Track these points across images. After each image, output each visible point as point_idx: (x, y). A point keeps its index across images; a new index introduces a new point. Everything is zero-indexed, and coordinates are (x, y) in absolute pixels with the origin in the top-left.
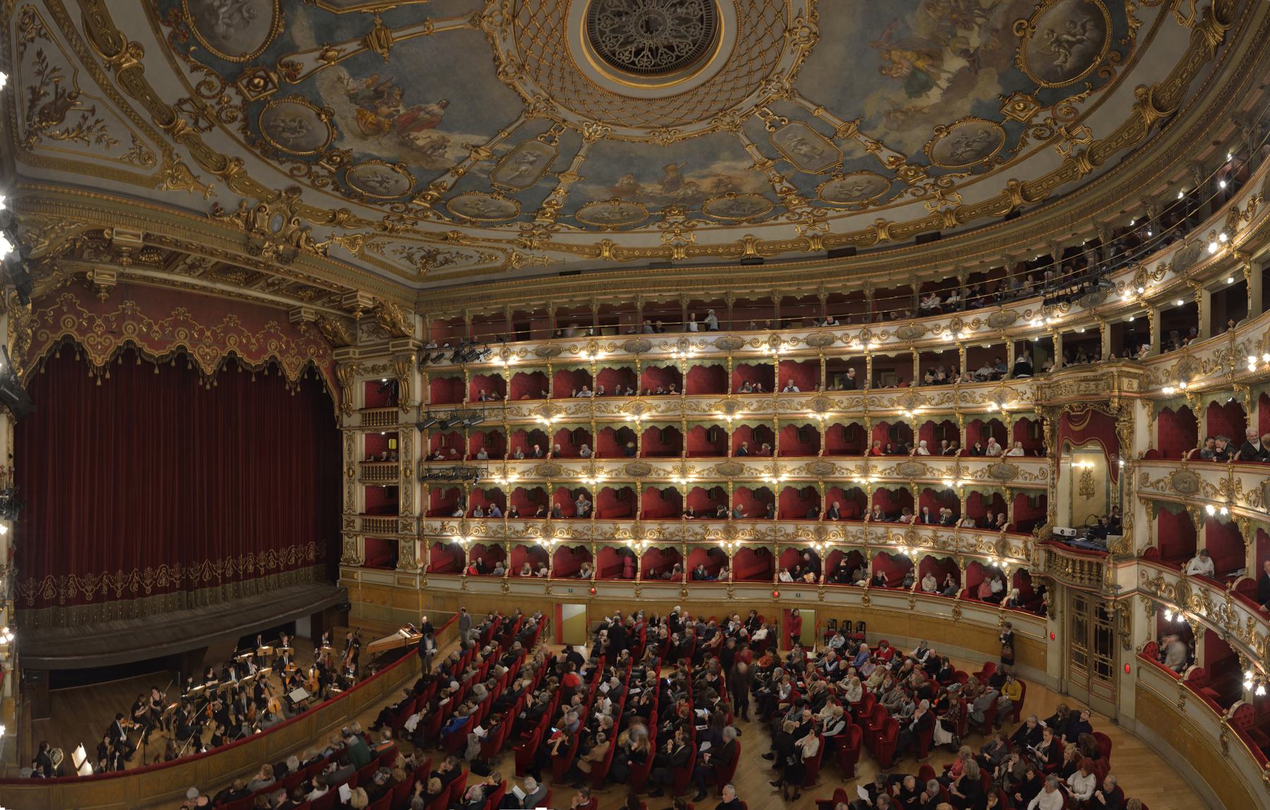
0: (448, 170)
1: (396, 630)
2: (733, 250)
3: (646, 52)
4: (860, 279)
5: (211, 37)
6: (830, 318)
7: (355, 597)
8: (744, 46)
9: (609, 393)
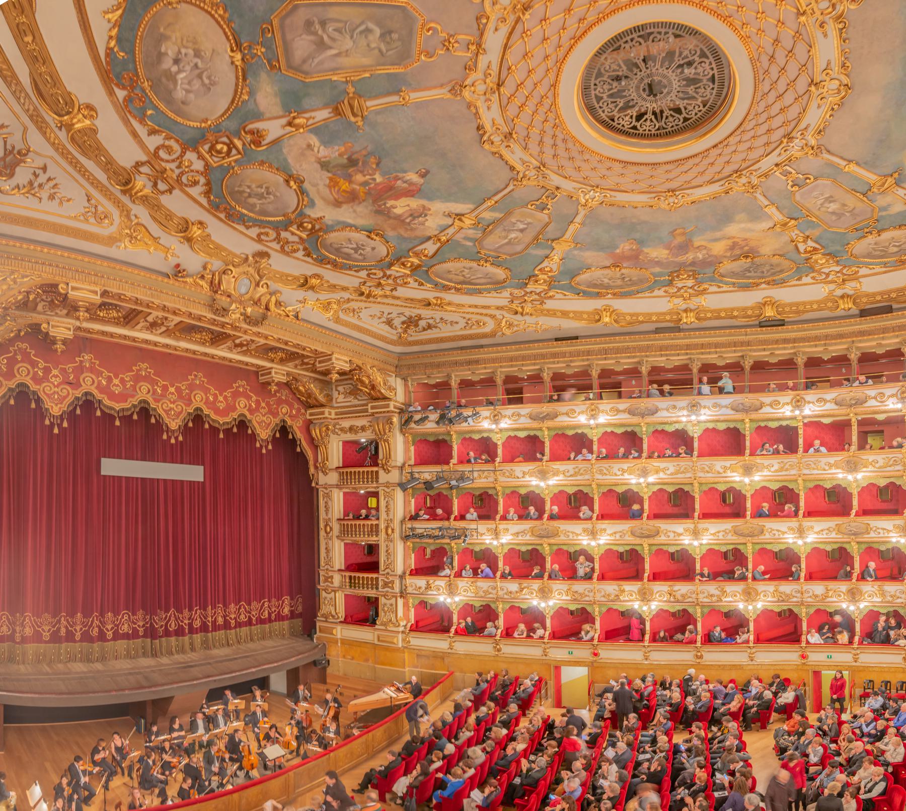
0: (429, 238)
1: (378, 689)
2: (750, 312)
3: (649, 116)
4: (897, 336)
5: (169, 101)
6: (862, 378)
7: (335, 654)
8: (763, 104)
9: (611, 456)
